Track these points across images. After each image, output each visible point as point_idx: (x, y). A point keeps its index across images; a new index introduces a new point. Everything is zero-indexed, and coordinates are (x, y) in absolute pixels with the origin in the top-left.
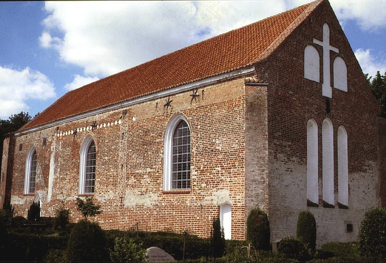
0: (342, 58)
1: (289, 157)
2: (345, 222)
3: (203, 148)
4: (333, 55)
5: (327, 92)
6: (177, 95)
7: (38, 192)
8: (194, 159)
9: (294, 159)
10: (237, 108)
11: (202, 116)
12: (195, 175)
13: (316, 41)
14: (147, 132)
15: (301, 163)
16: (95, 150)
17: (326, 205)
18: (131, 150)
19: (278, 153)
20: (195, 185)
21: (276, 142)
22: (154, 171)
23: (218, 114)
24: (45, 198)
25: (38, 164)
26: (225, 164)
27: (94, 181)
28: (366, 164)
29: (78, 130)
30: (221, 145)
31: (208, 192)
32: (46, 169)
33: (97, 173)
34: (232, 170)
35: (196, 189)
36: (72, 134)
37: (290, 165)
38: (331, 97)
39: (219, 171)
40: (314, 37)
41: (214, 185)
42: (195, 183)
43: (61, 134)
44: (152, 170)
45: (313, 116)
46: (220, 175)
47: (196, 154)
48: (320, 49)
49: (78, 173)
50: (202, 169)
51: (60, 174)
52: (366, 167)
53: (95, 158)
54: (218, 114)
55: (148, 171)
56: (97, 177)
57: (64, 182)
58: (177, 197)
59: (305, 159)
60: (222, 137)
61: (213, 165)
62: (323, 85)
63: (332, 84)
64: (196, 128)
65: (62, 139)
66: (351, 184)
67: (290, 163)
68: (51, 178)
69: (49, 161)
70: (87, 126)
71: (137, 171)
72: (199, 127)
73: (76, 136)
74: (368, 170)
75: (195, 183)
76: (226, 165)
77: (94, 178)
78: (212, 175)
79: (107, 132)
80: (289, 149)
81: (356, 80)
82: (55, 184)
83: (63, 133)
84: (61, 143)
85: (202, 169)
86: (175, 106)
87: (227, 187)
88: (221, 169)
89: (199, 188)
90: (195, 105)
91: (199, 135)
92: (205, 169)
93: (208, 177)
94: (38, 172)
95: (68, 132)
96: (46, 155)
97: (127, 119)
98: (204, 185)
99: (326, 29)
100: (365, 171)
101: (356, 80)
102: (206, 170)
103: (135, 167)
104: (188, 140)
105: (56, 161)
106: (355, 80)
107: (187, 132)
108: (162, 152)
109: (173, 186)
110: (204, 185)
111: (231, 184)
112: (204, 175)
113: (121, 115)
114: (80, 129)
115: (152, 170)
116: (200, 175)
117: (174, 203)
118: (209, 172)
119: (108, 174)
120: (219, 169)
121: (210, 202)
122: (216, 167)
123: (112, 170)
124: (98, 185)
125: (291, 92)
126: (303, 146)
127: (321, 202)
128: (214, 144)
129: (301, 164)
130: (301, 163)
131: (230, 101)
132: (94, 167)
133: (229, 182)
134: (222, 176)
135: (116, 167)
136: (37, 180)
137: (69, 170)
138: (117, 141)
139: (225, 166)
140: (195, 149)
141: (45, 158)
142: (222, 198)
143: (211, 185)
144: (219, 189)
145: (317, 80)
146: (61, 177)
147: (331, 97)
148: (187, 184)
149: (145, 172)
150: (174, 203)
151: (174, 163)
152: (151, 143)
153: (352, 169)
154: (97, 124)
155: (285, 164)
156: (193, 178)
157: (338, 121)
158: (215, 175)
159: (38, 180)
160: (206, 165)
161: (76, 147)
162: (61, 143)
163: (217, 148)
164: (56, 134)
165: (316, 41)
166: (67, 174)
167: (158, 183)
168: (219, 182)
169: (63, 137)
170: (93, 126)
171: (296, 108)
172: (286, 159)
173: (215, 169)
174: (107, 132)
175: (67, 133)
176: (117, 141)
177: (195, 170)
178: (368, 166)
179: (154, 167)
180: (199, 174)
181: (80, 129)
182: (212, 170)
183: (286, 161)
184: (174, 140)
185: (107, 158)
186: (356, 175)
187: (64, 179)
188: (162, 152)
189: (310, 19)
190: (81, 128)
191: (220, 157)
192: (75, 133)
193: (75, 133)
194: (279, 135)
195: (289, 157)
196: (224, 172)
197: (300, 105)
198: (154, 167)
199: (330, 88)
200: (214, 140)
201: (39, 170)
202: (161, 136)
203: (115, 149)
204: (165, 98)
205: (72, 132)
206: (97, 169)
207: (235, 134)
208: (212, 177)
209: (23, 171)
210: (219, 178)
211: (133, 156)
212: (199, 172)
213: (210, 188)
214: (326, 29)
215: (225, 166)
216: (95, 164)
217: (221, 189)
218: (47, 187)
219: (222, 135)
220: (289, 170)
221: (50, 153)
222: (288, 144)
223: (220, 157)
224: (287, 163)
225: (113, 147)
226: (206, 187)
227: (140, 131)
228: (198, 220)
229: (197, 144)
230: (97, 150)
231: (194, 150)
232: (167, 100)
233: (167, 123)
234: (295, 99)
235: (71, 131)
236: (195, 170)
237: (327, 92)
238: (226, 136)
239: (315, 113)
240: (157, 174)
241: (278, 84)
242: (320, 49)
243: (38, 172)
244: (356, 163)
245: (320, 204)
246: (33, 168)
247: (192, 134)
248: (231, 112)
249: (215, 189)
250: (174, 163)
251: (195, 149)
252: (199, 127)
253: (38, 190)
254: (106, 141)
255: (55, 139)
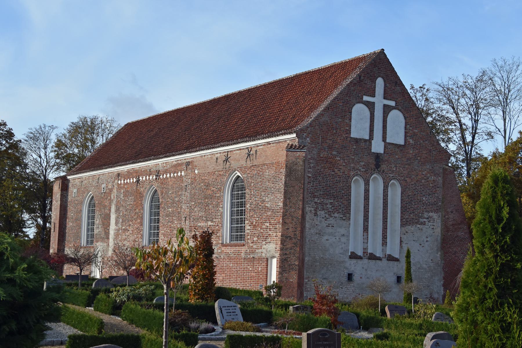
0: (399, 110)
1: (330, 213)
2: (394, 274)
3: (255, 204)
4: (387, 110)
5: (378, 147)
6: (234, 152)
7: (98, 244)
8: (248, 214)
9: (336, 215)
10: (282, 170)
11: (255, 174)
12: (249, 230)
13: (366, 98)
14: (208, 185)
15: (344, 218)
16: (159, 200)
17: (372, 257)
18: (193, 203)
19: (318, 210)
20: (248, 239)
21: (316, 201)
22: (215, 224)
23: (267, 173)
24: (105, 251)
25: (97, 214)
26: (272, 220)
27: (158, 233)
28: (426, 215)
29: (141, 178)
30: (269, 203)
31: (259, 245)
32: (107, 218)
33: (161, 224)
34: (278, 226)
35: (250, 242)
36: (134, 182)
37: (332, 221)
38: (382, 152)
39: (267, 227)
40: (364, 95)
41: (263, 239)
42: (249, 237)
43: (122, 182)
44: (212, 224)
45: (359, 173)
46: (268, 230)
47: (250, 210)
48: (371, 106)
49: (142, 224)
50: (254, 224)
51: (122, 225)
52: (425, 220)
53: (158, 237)
54: (267, 173)
55: (209, 225)
56: (161, 228)
57: (127, 234)
58: (233, 249)
59: (348, 215)
60: (270, 195)
61: (263, 221)
62: (373, 142)
63: (384, 139)
64: (250, 185)
65: (124, 187)
66: (403, 236)
67: (331, 219)
68: (112, 232)
69: (110, 210)
70: (150, 175)
71: (199, 224)
72: (252, 184)
73: (138, 184)
74: (427, 223)
75: (249, 237)
76: (273, 221)
77: (158, 230)
78: (262, 230)
79: (171, 183)
80: (331, 207)
81: (416, 131)
82: (117, 235)
83: (124, 181)
84: (122, 191)
85: (254, 224)
86: (232, 162)
87: (274, 241)
88: (270, 225)
89: (252, 241)
90: (249, 164)
91: (252, 192)
92: (257, 224)
93: (258, 232)
94: (98, 222)
95: (130, 180)
96: (106, 204)
97: (189, 171)
98: (255, 239)
99: (380, 83)
100: (424, 224)
101: (416, 131)
102: (257, 225)
103: (198, 219)
104: (243, 196)
105: (117, 210)
106: (415, 130)
107: (243, 188)
108: (221, 206)
109: (231, 240)
110: (255, 239)
111: (276, 238)
112: (256, 229)
113: (184, 166)
114: (142, 178)
115: (212, 224)
116: (253, 229)
117: (231, 255)
118: (260, 227)
119: (172, 225)
120: (268, 224)
121: (259, 255)
122: (266, 223)
123: (176, 222)
124: (163, 237)
125: (334, 153)
126: (346, 203)
127: (365, 255)
128: (264, 201)
129: (344, 220)
130: (344, 218)
131: (277, 162)
132: (158, 219)
133: (275, 236)
134: (270, 231)
135: (180, 219)
136: (96, 231)
137: (132, 221)
138: (180, 193)
139: (272, 222)
140: (249, 205)
141: (105, 207)
142: (270, 251)
143: (261, 239)
144: (267, 242)
145: (367, 137)
146: (124, 228)
147: (382, 152)
148: (241, 238)
149: (206, 225)
150: (231, 255)
151: (158, 238)
152: (211, 197)
153: (404, 223)
154: (161, 174)
155: (325, 220)
156: (247, 232)
157: (390, 175)
158: (265, 230)
159: (98, 231)
160: (257, 221)
161: (140, 196)
162: (122, 191)
163: (267, 205)
164: (116, 181)
165: (366, 98)
166: (130, 225)
167: (218, 236)
168: (268, 237)
169: (124, 184)
170: (157, 176)
171: (340, 167)
172: (327, 215)
173: (264, 225)
174: (171, 183)
175: (128, 181)
176: (180, 193)
177: (248, 225)
178: (427, 218)
179: (214, 220)
180: (252, 228)
181: (142, 178)
182: (263, 225)
183: (327, 217)
184: (232, 195)
185: (170, 210)
186: (410, 228)
187: (126, 230)
188: (221, 206)
189: (360, 78)
190: (144, 177)
191: (269, 213)
192: (138, 181)
193: (138, 181)
194: (320, 194)
195: (330, 213)
196: (271, 227)
197: (344, 164)
198: (214, 220)
199: (383, 143)
200: (264, 198)
201: (98, 219)
202: (220, 191)
203: (179, 201)
204: (224, 154)
205: (135, 180)
206: (161, 220)
207: (280, 193)
208: (262, 231)
209: (78, 220)
210: (268, 233)
211: (196, 209)
212: (252, 226)
213: (260, 242)
214: (380, 83)
215: (272, 222)
216: (158, 214)
217: (269, 243)
218: (108, 238)
219: (270, 193)
220: (330, 225)
221: (111, 201)
222: (330, 201)
223: (269, 213)
224: (328, 219)
225: (176, 199)
226: (258, 241)
227: (202, 184)
228: (251, 271)
229: (251, 201)
230: (161, 200)
231: (248, 206)
232: (226, 156)
233: (226, 178)
234: (339, 159)
235: (133, 179)
236: (248, 225)
237: (378, 147)
238: (273, 195)
239: (362, 170)
240: (217, 228)
241: (320, 147)
242: (371, 106)
243: (98, 222)
244: (412, 215)
245: (364, 256)
246: (91, 218)
247: (247, 191)
248: (278, 173)
249: (264, 243)
250: (158, 238)
251: (249, 205)
252: (252, 184)
253: (97, 242)
254: (170, 192)
255: (116, 186)
